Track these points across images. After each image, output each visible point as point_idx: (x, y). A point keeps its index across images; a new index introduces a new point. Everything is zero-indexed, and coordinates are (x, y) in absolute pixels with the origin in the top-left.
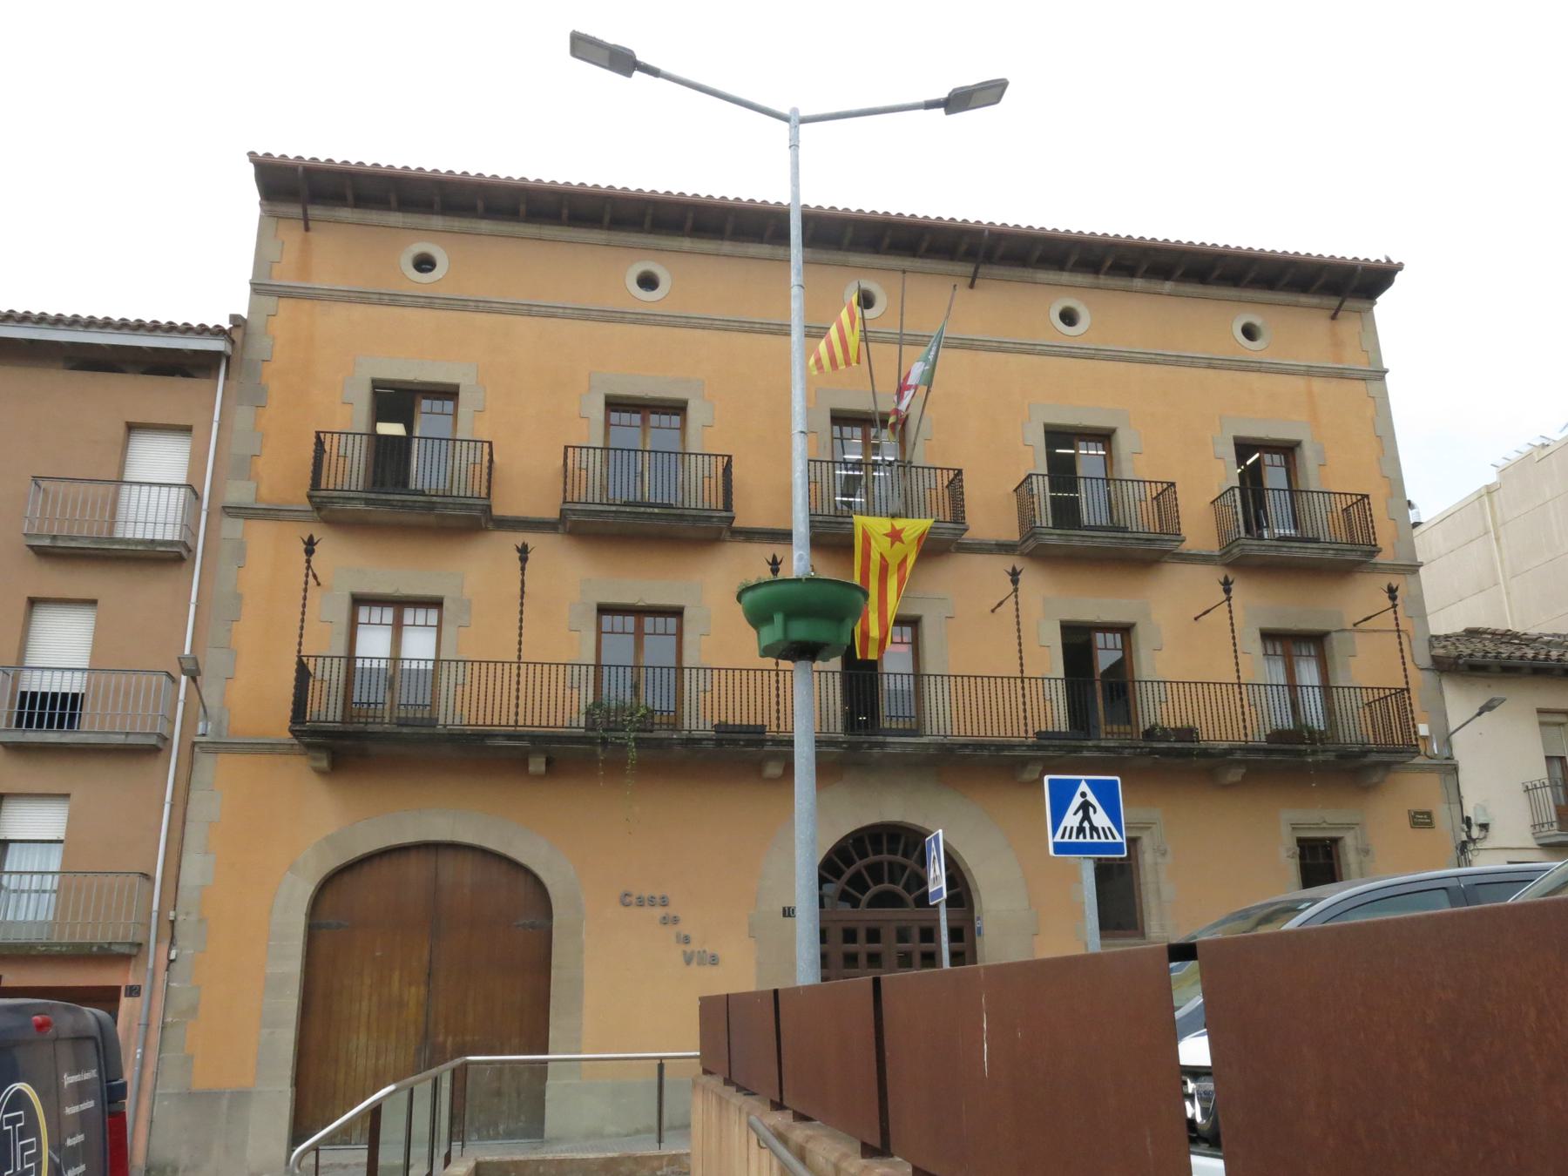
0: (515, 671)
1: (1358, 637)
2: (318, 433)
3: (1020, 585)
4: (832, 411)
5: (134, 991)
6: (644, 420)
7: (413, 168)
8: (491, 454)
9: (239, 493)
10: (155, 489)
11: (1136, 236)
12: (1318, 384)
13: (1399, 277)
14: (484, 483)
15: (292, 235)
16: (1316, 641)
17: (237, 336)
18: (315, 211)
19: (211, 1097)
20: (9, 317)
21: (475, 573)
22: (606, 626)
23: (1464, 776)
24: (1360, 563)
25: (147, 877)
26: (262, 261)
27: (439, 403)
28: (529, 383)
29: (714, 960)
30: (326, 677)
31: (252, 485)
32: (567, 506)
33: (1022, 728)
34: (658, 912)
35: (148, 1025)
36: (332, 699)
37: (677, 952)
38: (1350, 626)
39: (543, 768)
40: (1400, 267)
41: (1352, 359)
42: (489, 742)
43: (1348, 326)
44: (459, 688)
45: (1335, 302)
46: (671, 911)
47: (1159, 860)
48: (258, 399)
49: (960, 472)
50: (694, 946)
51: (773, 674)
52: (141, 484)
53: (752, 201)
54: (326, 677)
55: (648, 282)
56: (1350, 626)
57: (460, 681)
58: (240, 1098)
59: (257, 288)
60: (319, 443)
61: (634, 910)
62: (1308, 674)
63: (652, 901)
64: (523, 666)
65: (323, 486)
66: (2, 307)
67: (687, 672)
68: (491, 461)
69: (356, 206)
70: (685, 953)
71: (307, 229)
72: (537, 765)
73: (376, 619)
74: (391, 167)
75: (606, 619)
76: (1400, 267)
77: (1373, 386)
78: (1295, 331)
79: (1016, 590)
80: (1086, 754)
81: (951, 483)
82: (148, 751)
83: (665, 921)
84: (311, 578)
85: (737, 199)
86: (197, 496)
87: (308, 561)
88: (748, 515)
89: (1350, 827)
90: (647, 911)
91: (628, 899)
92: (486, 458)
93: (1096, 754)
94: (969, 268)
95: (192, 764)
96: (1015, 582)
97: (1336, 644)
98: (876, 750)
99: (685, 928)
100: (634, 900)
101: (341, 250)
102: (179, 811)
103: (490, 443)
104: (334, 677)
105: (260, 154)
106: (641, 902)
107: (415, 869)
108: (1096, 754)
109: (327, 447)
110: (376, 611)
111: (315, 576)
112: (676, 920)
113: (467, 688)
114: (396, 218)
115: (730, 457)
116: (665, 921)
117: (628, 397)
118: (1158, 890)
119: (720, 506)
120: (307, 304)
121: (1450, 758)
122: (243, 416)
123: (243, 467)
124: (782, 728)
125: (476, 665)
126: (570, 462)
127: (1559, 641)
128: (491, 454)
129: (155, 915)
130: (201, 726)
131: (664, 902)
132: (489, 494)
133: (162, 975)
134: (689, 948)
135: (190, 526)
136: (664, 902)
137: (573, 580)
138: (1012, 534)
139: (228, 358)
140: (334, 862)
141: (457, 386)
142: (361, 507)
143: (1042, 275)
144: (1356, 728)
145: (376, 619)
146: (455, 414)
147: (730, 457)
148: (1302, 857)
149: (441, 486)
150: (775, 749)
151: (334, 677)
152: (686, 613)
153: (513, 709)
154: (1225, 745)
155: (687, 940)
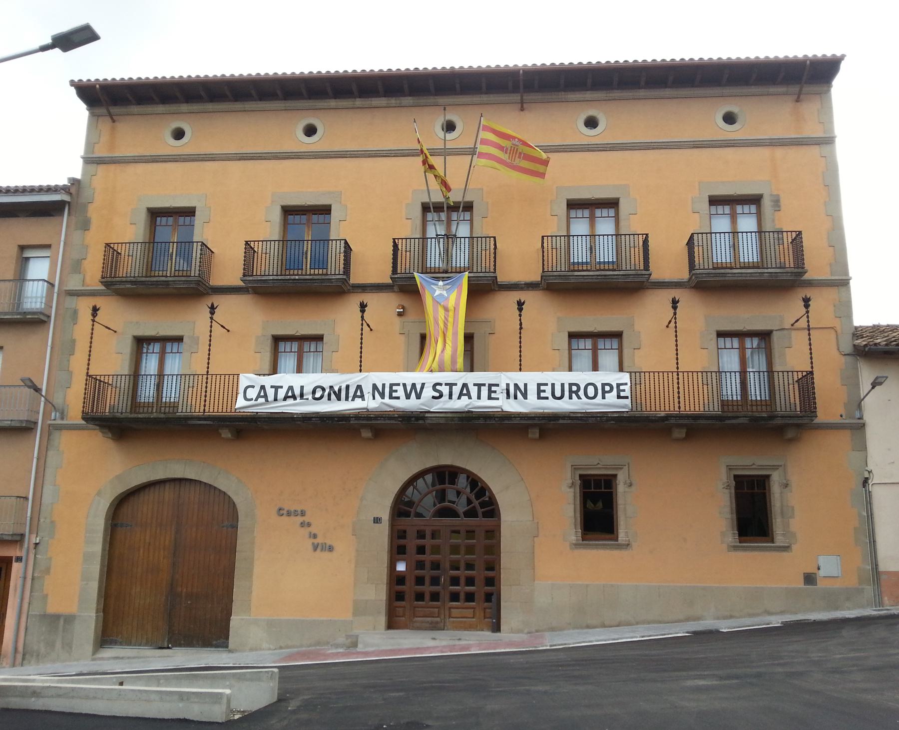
0: (205, 380)
1: (794, 333)
2: (394, 239)
3: (810, 309)
4: (710, 197)
5: (19, 559)
6: (176, 222)
7: (333, 71)
8: (495, 245)
9: (74, 284)
10: (36, 282)
11: (696, 59)
12: (779, 152)
13: (843, 65)
14: (492, 263)
15: (105, 125)
16: (765, 336)
17: (73, 190)
18: (114, 110)
19: (56, 617)
20: (8, 191)
21: (646, 318)
22: (721, 345)
23: (870, 432)
24: (794, 281)
25: (26, 498)
26: (90, 144)
27: (322, 217)
28: (237, 205)
29: (331, 549)
30: (118, 385)
31: (81, 276)
32: (546, 274)
33: (677, 405)
34: (300, 519)
35: (25, 578)
36: (121, 397)
37: (309, 543)
38: (788, 326)
39: (538, 435)
40: (842, 57)
41: (811, 130)
42: (189, 422)
43: (809, 108)
44: (191, 389)
45: (795, 89)
46: (306, 519)
47: (627, 490)
48: (85, 225)
49: (800, 233)
50: (319, 540)
51: (675, 374)
52: (33, 280)
53: (198, 76)
54: (118, 385)
55: (591, 123)
56: (789, 326)
57: (191, 385)
58: (69, 619)
59: (89, 160)
60: (395, 246)
61: (285, 518)
62: (757, 363)
63: (296, 513)
64: (681, 374)
65: (399, 271)
66: (4, 184)
67: (776, 374)
68: (495, 248)
69: (187, 102)
70: (313, 544)
71: (114, 121)
72: (679, 433)
73: (728, 345)
74: (267, 74)
75: (574, 341)
76: (842, 57)
77: (825, 149)
78: (765, 116)
79: (807, 312)
80: (561, 421)
81: (793, 240)
82: (24, 429)
83: (302, 524)
84: (365, 324)
85: (691, 59)
86: (53, 285)
87: (362, 317)
88: (658, 273)
89: (775, 468)
90: (293, 518)
91: (282, 512)
92: (492, 247)
93: (569, 422)
94: (516, 97)
95: (49, 435)
96: (675, 308)
97: (775, 336)
98: (420, 422)
99: (313, 529)
100: (285, 512)
101: (146, 134)
102: (42, 461)
103: (495, 238)
104: (123, 385)
105: (76, 80)
106: (289, 514)
107: (168, 493)
108: (569, 422)
109: (400, 247)
110: (288, 344)
111: (676, 323)
112: (309, 525)
113: (195, 389)
114: (161, 108)
115: (647, 235)
116: (302, 524)
117: (185, 208)
118: (625, 509)
119: (642, 268)
120: (112, 167)
121: (861, 418)
122: (77, 235)
123: (76, 266)
124: (682, 409)
125: (192, 377)
126: (545, 245)
127: (894, 328)
128: (495, 245)
129: (28, 519)
130: (53, 414)
131: (303, 513)
132: (495, 269)
133: (32, 552)
134: (316, 541)
135: (49, 305)
136: (303, 513)
137: (699, 316)
138: (683, 274)
139: (69, 203)
140: (121, 489)
141: (195, 208)
142: (129, 286)
143: (572, 96)
144: (789, 399)
145: (608, 346)
146: (471, 221)
147: (647, 235)
148: (736, 488)
149: (458, 265)
150: (356, 422)
151: (123, 385)
152: (624, 335)
153: (676, 400)
154: (663, 414)
155: (315, 536)
